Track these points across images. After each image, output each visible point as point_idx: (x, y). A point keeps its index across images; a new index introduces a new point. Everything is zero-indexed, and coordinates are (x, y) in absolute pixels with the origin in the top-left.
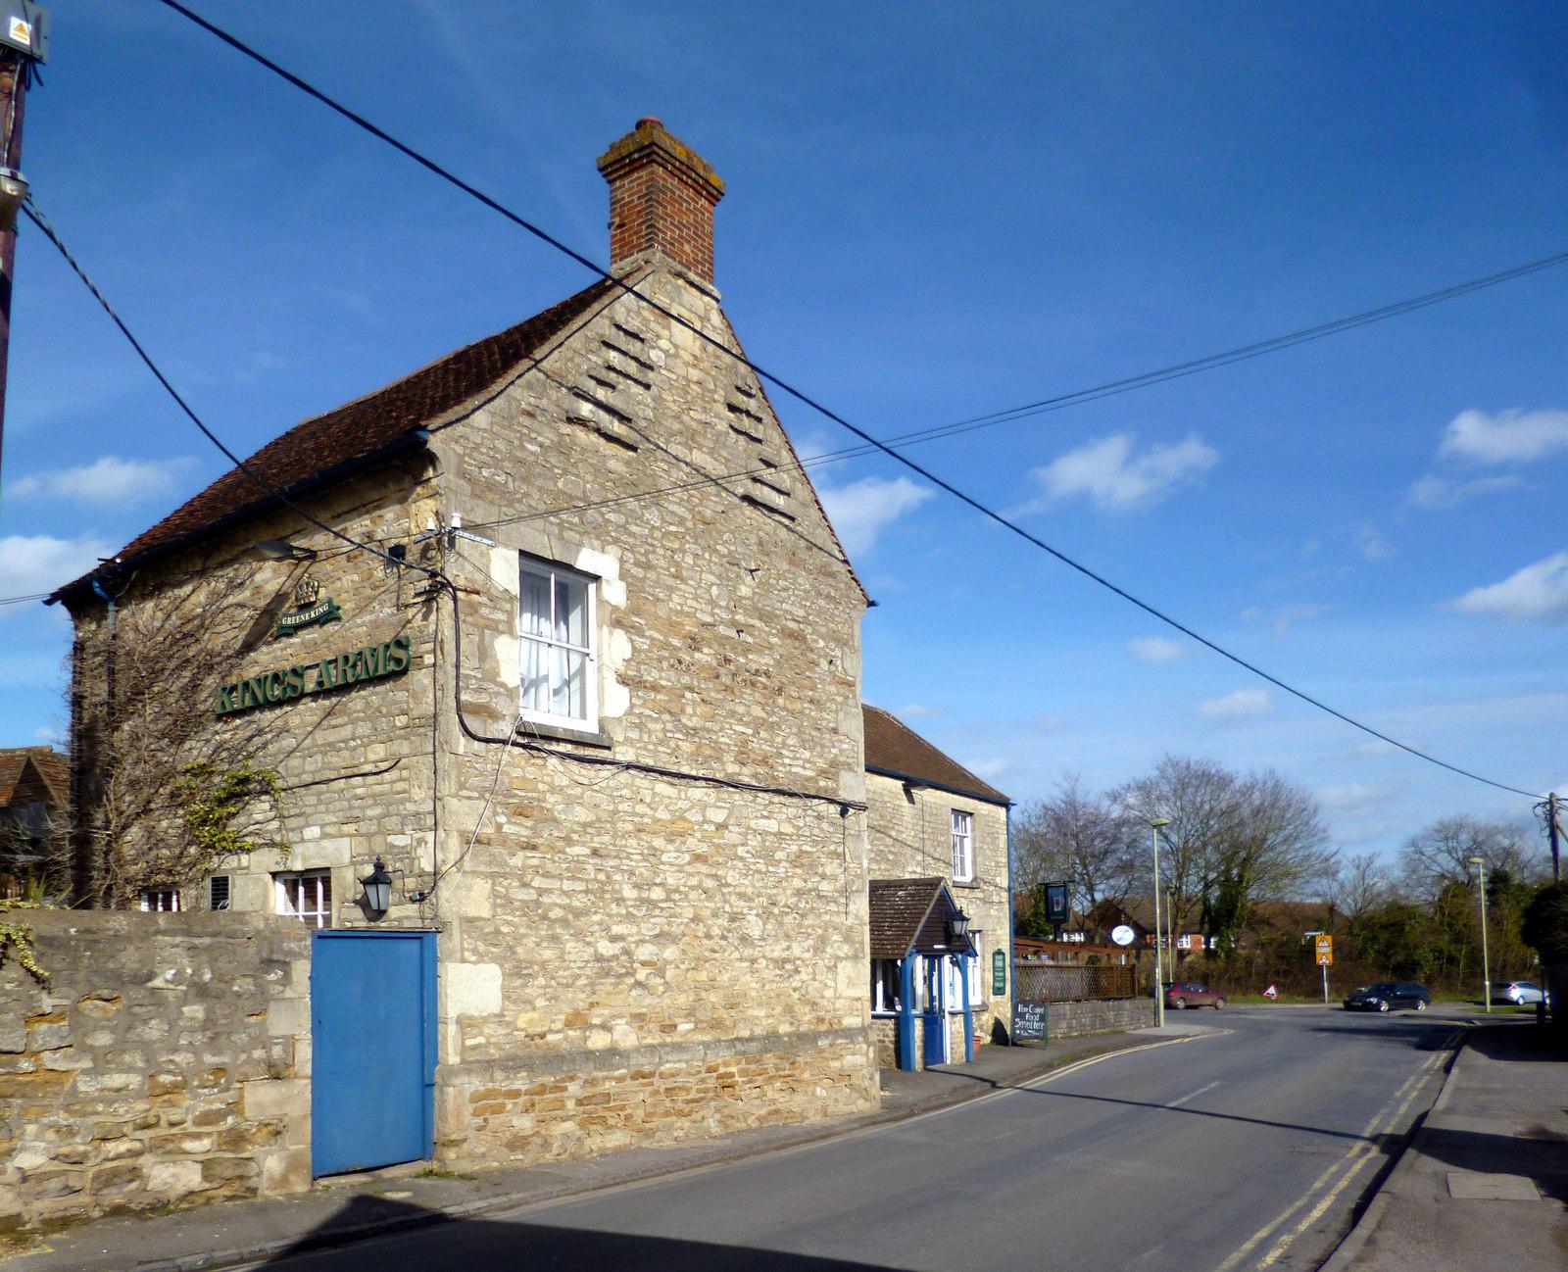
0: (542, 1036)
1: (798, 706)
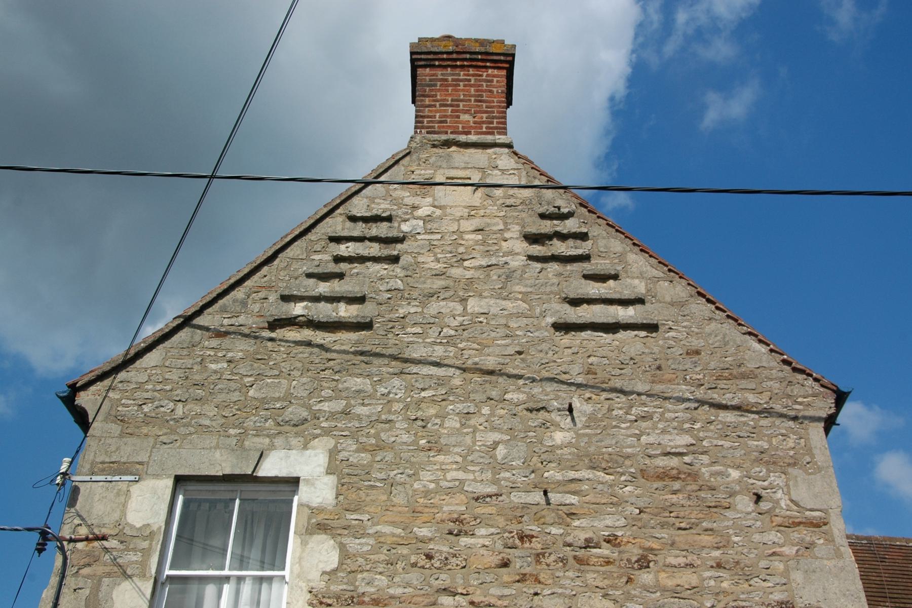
1: (687, 578)
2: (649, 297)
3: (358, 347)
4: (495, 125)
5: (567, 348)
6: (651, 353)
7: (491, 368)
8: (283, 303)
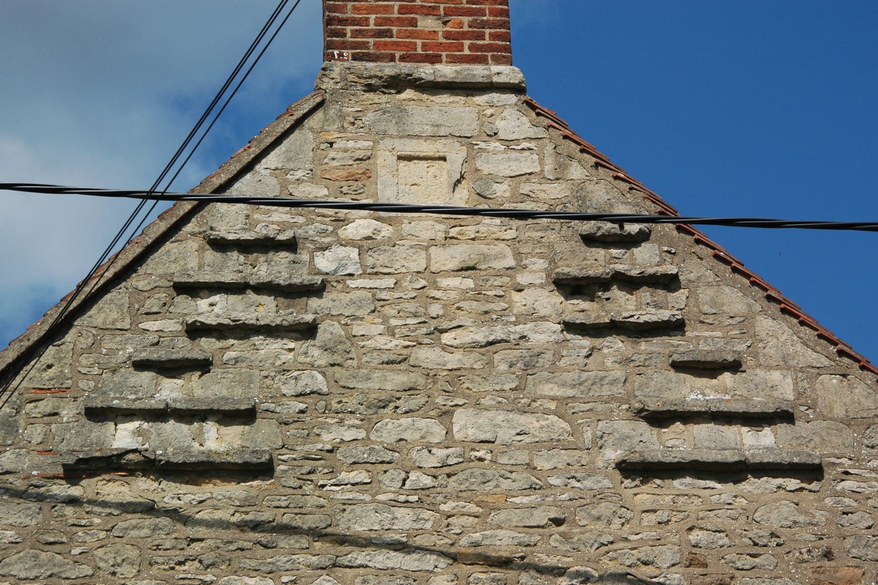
2: (803, 408)
3: (247, 513)
4: (487, 41)
5: (647, 511)
6: (811, 524)
7: (505, 554)
8: (92, 424)
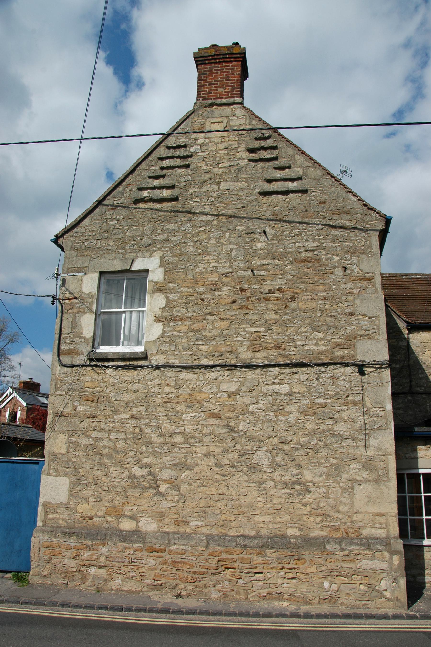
0: (91, 518)
4: (235, 93)
